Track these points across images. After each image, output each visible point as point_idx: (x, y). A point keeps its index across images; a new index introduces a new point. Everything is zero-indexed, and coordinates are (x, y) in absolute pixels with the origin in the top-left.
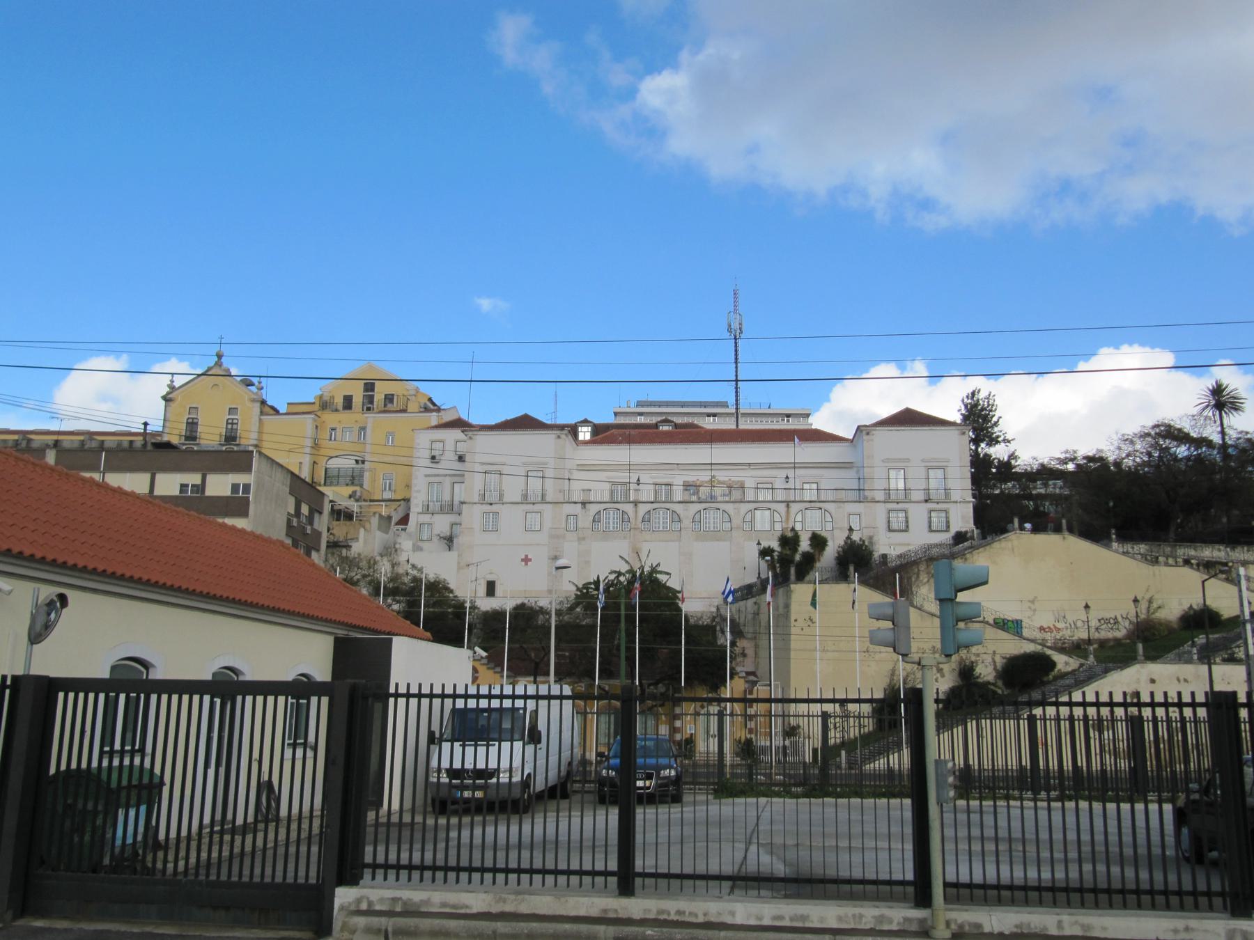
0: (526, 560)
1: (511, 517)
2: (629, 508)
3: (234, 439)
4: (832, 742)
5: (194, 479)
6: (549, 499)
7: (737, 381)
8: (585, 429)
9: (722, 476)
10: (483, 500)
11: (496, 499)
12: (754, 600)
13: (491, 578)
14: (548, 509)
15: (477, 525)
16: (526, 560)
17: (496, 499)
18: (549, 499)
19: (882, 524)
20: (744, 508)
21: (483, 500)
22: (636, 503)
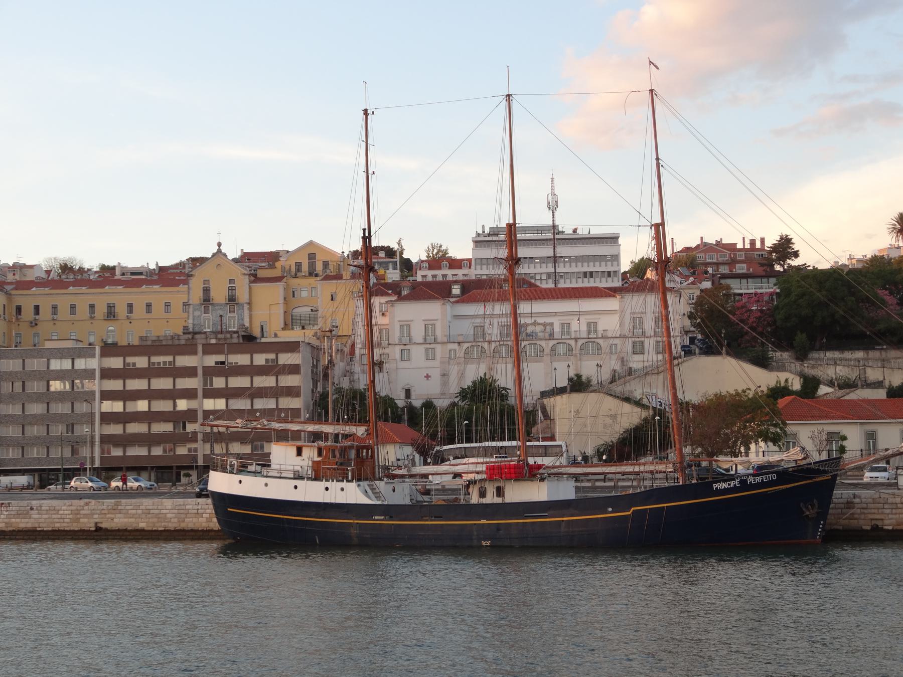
0: (428, 376)
1: (418, 353)
2: (486, 345)
3: (234, 300)
4: (215, 524)
5: (272, 356)
6: (439, 341)
7: (555, 257)
8: (456, 287)
9: (540, 320)
10: (401, 343)
11: (408, 342)
12: (484, 501)
13: (407, 387)
14: (438, 348)
15: (398, 356)
16: (428, 376)
17: (408, 342)
18: (439, 341)
19: (630, 350)
20: (552, 343)
21: (401, 343)
22: (489, 342)
